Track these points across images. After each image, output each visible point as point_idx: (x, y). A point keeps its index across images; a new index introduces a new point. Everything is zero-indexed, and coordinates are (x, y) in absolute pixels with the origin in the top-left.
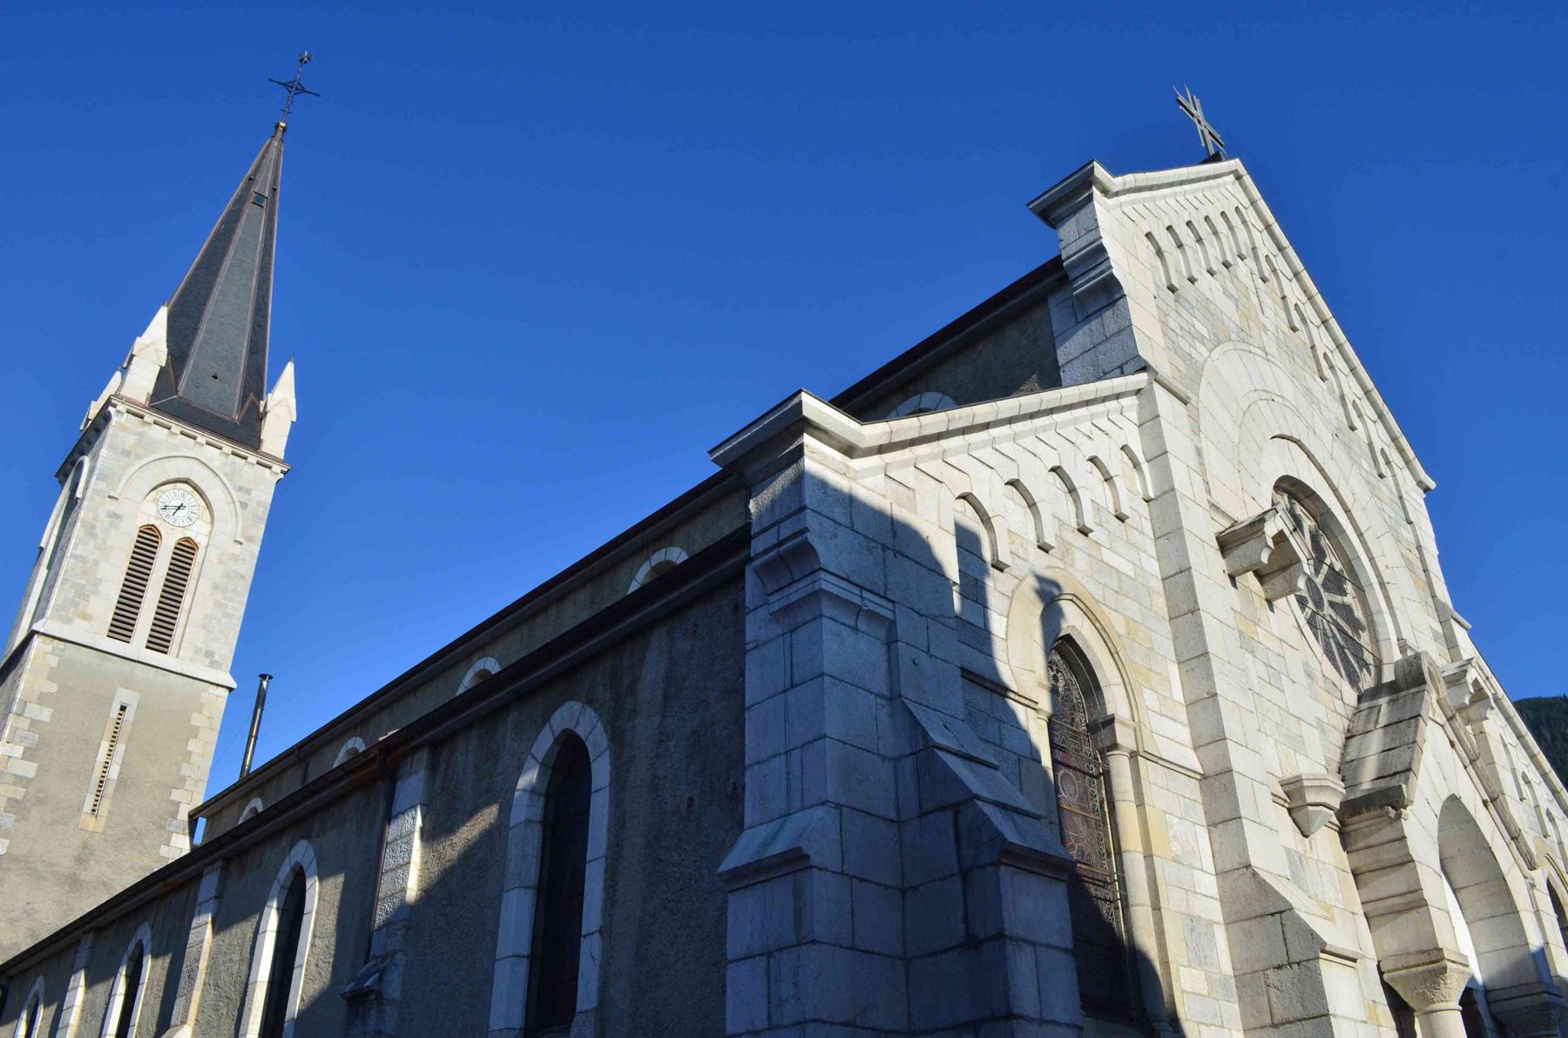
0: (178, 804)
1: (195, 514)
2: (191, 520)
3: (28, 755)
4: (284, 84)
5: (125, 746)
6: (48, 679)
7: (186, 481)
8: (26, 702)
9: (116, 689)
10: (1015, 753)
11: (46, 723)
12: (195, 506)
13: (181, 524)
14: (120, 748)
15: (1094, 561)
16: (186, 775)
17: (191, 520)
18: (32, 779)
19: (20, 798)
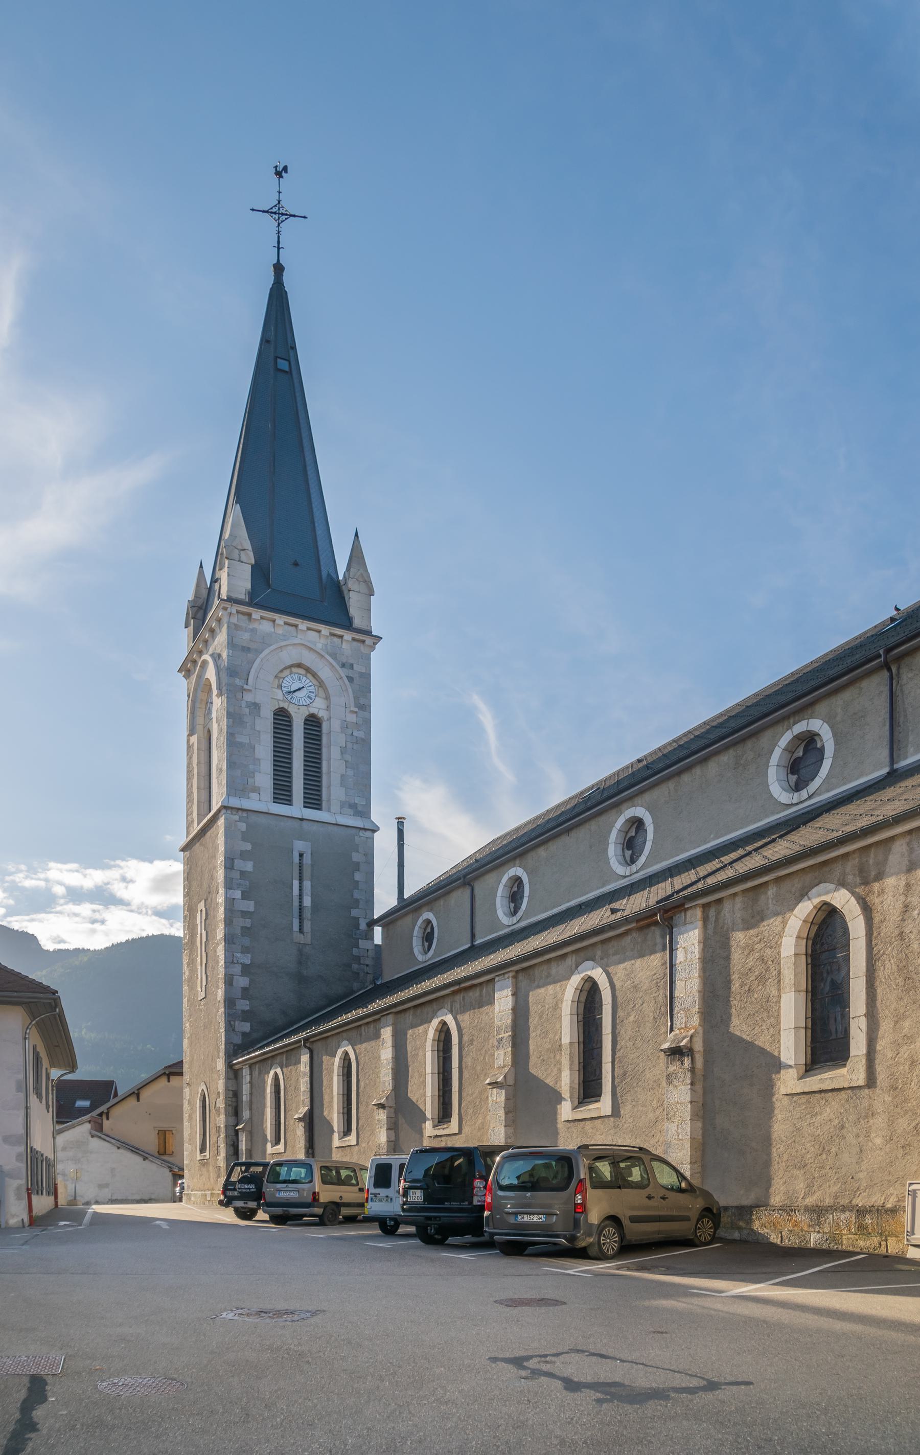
1: (313, 693)
2: (311, 698)
3: (245, 896)
7: (299, 665)
8: (233, 859)
13: (305, 704)
14: (307, 884)
17: (311, 698)
19: (249, 926)
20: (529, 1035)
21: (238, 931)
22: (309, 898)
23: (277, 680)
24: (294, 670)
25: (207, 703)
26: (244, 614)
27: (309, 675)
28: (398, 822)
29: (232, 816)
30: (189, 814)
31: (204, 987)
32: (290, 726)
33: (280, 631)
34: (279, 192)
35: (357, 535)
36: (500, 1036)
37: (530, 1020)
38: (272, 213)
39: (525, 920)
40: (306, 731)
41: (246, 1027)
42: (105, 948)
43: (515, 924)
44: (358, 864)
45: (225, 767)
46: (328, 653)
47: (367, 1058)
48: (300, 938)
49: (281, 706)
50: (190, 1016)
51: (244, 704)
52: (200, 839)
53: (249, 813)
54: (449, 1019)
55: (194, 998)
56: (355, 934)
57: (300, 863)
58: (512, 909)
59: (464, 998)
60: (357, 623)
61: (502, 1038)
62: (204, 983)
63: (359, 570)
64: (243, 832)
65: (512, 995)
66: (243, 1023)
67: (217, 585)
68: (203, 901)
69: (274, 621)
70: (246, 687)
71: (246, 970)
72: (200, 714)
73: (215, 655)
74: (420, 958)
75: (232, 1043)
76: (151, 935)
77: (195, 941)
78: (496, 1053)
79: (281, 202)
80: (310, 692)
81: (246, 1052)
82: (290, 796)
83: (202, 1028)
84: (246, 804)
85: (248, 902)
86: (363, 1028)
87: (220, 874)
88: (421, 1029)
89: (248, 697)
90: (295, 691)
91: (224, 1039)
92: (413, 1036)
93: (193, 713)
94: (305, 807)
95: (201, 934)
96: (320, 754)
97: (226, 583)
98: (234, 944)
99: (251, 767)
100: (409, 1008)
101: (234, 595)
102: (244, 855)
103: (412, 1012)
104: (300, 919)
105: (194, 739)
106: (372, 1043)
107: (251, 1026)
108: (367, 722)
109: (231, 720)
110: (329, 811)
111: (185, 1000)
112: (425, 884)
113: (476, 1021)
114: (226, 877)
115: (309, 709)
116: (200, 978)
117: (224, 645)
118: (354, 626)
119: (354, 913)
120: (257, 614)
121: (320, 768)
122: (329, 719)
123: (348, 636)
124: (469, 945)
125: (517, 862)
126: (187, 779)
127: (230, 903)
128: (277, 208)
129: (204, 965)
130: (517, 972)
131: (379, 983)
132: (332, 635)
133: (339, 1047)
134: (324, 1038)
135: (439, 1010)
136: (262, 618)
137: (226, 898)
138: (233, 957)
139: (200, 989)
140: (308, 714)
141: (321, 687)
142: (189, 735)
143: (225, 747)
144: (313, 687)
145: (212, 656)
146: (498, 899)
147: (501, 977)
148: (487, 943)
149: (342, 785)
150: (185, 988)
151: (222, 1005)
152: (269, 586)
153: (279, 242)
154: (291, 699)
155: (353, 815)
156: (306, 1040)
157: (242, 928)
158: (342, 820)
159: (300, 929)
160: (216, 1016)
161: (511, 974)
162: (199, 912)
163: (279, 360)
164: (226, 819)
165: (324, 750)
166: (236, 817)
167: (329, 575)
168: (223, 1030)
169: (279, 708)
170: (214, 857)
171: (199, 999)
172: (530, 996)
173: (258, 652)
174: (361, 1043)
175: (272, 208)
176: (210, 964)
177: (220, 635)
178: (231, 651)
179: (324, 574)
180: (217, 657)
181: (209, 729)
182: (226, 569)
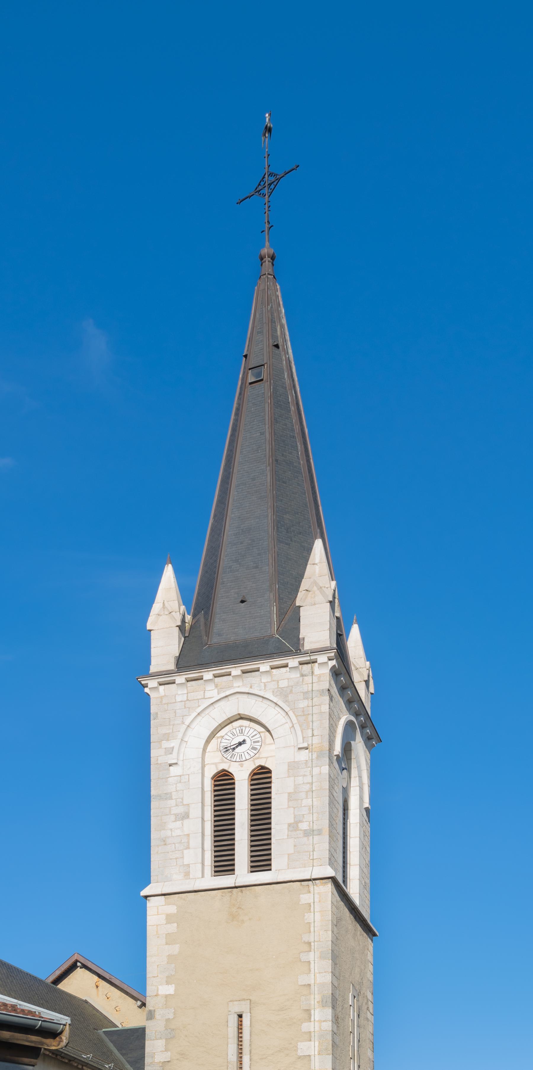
10: (154, 925)
12: (256, 735)
15: (334, 986)
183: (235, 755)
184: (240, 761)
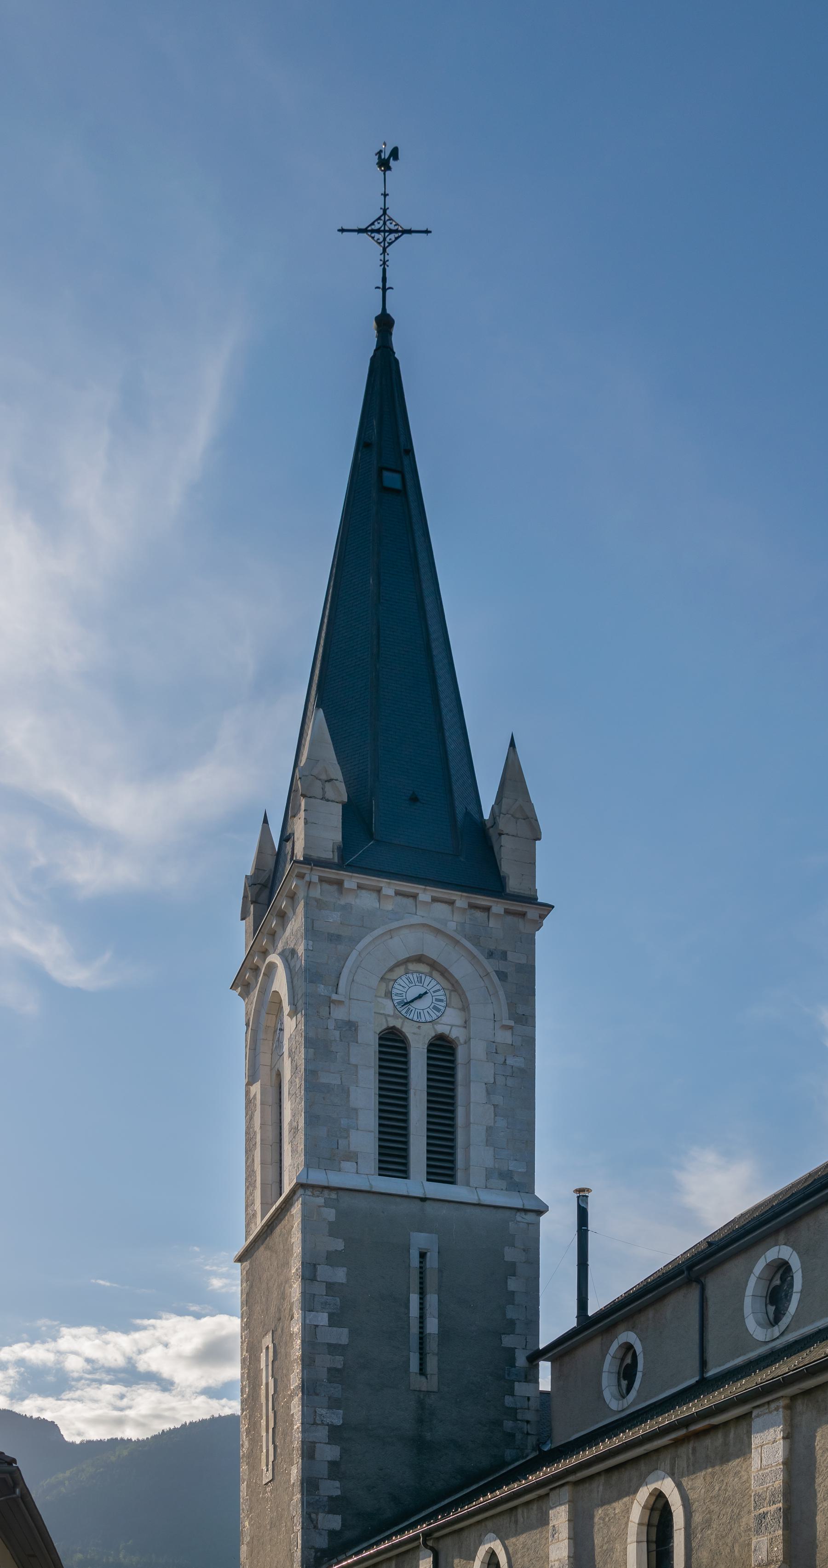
0: (513, 1350)
1: (441, 1001)
2: (438, 1010)
3: (334, 1320)
4: (365, 231)
5: (436, 1296)
6: (330, 1236)
7: (420, 959)
8: (315, 1265)
9: (409, 1235)
11: (342, 1284)
12: (439, 990)
13: (429, 1019)
14: (432, 1299)
16: (514, 1318)
17: (438, 1010)
18: (348, 1344)
19: (340, 1367)
20: (816, 1505)
21: (324, 1375)
22: (436, 1321)
23: (384, 985)
24: (412, 966)
25: (275, 1031)
26: (330, 882)
27: (435, 974)
28: (578, 1197)
29: (313, 1199)
30: (249, 1204)
31: (270, 1463)
32: (406, 1056)
33: (389, 906)
34: (385, 195)
35: (512, 744)
36: (761, 1511)
37: (818, 1481)
38: (373, 231)
39: (795, 1330)
40: (432, 1062)
41: (335, 1522)
42: (152, 1437)
43: (778, 1338)
44: (513, 1265)
45: (302, 1124)
46: (465, 937)
47: (526, 1559)
48: (421, 1383)
49: (391, 1025)
50: (251, 1509)
51: (331, 1025)
52: (266, 1239)
53: (341, 1193)
54: (668, 1486)
55: (256, 1482)
56: (509, 1375)
57: (421, 1268)
58: (771, 1316)
59: (694, 1450)
60: (513, 885)
61: (765, 1515)
62: (271, 1458)
63: (516, 800)
64: (330, 1223)
65: (784, 1438)
66: (330, 1516)
67: (289, 845)
68: (270, 1334)
69: (379, 891)
70: (334, 997)
71: (335, 1434)
72: (265, 1048)
73: (287, 953)
74: (614, 1405)
75: (313, 1547)
76: (216, 1415)
77: (259, 1396)
78: (754, 1541)
79: (388, 212)
80: (437, 1000)
81: (335, 1560)
82: (406, 1164)
83: (269, 1527)
84: (335, 1179)
85: (341, 1329)
86: (520, 1511)
87: (296, 1290)
88: (618, 1506)
89: (339, 1013)
90: (412, 1001)
91: (300, 1542)
92: (604, 1520)
93: (255, 1049)
94: (428, 1180)
95: (267, 1384)
96: (453, 1097)
97: (303, 836)
98: (317, 1395)
99: (344, 1122)
100: (599, 1474)
101: (315, 854)
102: (332, 1259)
103: (602, 1479)
104: (421, 1354)
105: (256, 1089)
106: (535, 1534)
107: (343, 1520)
108: (530, 1042)
109: (312, 1050)
110: (468, 1184)
111: (244, 1486)
112: (622, 1293)
113: (717, 1488)
114: (303, 1293)
115: (435, 1026)
116: (265, 1451)
117: (299, 935)
118: (508, 891)
119: (508, 1341)
120: (351, 881)
121: (453, 1119)
122: (468, 1041)
123: (498, 907)
124: (697, 1379)
125: (782, 1236)
126: (246, 1152)
127: (310, 1332)
128: (381, 222)
129: (271, 1431)
130: (793, 1398)
131: (546, 1449)
132: (472, 906)
133: (481, 1543)
134: (457, 1531)
135: (650, 1473)
136: (360, 887)
137: (304, 1326)
138: (315, 1415)
139: (264, 1468)
140: (433, 1034)
141: (455, 991)
142: (249, 1084)
143: (303, 1092)
144: (442, 992)
145: (282, 955)
146: (748, 1301)
147: (762, 1409)
148: (727, 1373)
149: (488, 1143)
150: (244, 1467)
151: (297, 1489)
152: (371, 836)
153: (384, 279)
154: (406, 1012)
155: (506, 1190)
156: (427, 1535)
157: (330, 1370)
158: (488, 1198)
159: (421, 1370)
160: (289, 1507)
161: (782, 1403)
162: (264, 1351)
163: (386, 474)
164: (303, 1204)
165: (460, 1091)
166: (320, 1201)
167: (467, 814)
168: (299, 1527)
169: (388, 1028)
170: (286, 1264)
171: (264, 1483)
172: (818, 1438)
173: (354, 941)
174: (516, 1534)
175: (373, 224)
176: (280, 1429)
177: (293, 920)
178: (311, 943)
179: (460, 811)
180: (289, 956)
181: (278, 1070)
182: (302, 814)
183: (412, 1010)
184: (418, 1020)
